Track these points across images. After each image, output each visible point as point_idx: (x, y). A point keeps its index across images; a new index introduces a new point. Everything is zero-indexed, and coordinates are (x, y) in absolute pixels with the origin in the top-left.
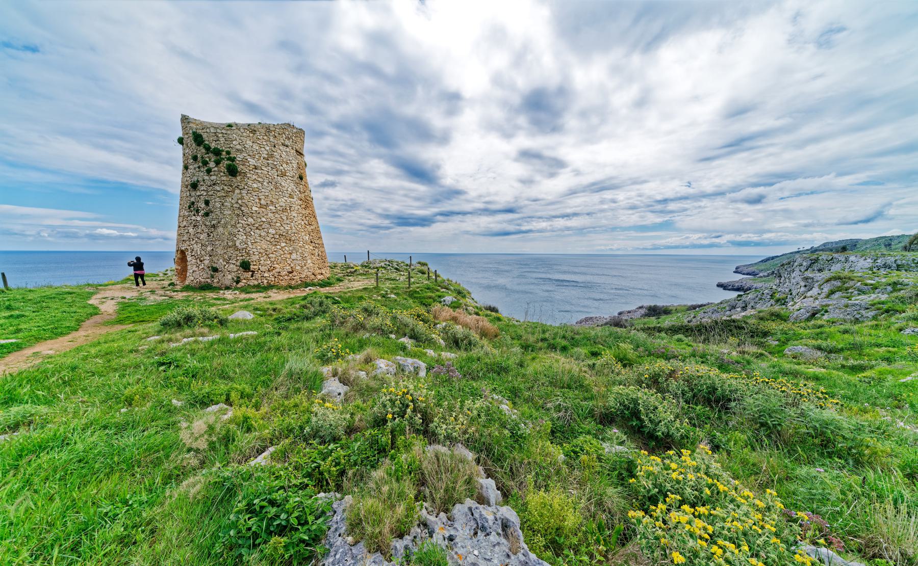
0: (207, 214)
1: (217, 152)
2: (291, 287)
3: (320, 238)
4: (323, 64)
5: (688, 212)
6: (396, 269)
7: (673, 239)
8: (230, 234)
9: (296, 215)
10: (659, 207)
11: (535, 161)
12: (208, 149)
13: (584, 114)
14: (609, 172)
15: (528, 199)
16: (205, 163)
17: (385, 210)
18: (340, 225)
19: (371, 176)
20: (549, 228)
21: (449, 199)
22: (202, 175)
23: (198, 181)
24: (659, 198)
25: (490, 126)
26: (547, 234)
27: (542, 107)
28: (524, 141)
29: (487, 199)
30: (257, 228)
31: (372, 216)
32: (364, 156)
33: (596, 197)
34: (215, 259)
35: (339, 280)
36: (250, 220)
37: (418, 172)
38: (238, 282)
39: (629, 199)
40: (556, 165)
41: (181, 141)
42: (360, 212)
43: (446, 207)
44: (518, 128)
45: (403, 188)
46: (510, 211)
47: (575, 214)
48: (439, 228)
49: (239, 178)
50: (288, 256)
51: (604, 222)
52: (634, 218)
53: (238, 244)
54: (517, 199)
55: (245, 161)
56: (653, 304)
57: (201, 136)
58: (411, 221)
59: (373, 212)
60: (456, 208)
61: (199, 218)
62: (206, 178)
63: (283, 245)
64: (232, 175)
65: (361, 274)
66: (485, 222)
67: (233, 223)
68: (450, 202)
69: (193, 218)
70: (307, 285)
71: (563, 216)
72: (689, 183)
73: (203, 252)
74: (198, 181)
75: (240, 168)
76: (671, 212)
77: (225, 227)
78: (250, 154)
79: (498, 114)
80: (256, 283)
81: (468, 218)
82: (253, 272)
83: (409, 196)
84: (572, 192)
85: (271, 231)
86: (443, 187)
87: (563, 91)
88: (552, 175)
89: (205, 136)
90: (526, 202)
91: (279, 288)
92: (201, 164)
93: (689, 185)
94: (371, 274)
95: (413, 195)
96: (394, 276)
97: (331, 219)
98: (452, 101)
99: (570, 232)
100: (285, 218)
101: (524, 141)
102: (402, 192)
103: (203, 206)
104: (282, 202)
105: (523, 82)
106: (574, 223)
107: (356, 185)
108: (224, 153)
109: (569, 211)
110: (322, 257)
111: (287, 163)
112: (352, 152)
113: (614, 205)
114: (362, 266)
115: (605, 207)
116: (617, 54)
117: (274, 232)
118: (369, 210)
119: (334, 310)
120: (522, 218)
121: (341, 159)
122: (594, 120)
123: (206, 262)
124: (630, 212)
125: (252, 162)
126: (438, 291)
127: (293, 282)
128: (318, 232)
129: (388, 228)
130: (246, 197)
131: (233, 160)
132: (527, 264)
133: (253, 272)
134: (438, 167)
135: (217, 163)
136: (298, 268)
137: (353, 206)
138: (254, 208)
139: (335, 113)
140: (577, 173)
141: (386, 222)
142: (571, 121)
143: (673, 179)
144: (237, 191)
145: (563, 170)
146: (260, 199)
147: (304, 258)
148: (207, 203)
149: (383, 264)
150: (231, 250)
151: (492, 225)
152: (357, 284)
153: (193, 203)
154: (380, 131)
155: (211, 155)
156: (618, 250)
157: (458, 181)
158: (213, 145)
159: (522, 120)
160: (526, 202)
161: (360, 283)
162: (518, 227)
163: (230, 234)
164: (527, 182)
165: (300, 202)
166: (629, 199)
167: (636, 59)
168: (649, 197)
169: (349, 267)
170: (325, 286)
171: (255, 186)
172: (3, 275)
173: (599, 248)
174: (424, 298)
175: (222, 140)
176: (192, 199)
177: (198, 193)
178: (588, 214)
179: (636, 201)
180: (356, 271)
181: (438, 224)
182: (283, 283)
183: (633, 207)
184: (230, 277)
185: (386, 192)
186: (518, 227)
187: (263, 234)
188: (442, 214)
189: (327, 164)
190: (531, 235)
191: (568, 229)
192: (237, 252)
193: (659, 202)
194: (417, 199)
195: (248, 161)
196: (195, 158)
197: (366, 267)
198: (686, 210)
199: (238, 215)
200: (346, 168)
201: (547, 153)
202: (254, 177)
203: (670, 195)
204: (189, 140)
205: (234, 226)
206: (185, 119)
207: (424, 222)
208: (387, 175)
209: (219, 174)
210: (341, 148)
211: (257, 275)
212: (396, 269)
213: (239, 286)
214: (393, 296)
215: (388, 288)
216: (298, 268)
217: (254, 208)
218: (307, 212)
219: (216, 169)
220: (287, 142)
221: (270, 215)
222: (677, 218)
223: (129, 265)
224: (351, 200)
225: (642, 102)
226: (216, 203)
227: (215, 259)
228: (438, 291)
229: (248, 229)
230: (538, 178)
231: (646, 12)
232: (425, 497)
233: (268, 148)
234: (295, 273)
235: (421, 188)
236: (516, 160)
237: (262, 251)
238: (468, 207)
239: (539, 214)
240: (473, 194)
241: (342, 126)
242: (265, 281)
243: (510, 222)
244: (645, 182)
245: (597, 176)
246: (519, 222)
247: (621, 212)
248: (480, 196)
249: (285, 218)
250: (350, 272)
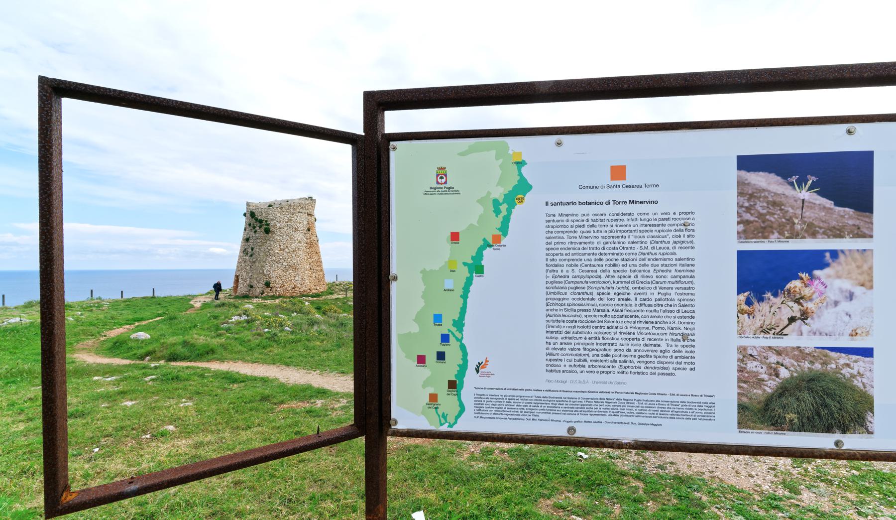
0: (251, 256)
1: (261, 221)
12: (256, 219)
16: (254, 227)
22: (252, 234)
75: (272, 229)
77: (259, 262)
78: (277, 220)
125: (278, 225)
131: (268, 225)
135: (260, 227)
147: (303, 279)
148: (252, 249)
150: (261, 276)
155: (259, 223)
172: (3, 296)
195: (275, 224)
196: (250, 225)
204: (248, 215)
205: (264, 262)
206: (248, 204)
209: (261, 233)
211: (274, 290)
223: (465, 264)
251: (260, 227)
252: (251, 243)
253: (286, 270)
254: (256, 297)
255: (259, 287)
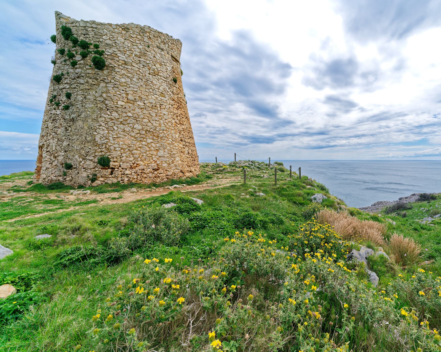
0: (67, 108)
1: (85, 46)
2: (155, 185)
3: (192, 138)
4: (208, 49)
5: (437, 133)
6: (258, 168)
7: (428, 150)
8: (90, 128)
9: (166, 113)
10: (417, 130)
11: (337, 103)
12: (75, 42)
13: (365, 75)
14: (382, 109)
15: (333, 126)
16: (71, 56)
17: (244, 133)
18: (216, 143)
19: (236, 113)
20: (347, 144)
21: (283, 126)
23: (62, 75)
24: (416, 124)
25: (308, 82)
26: (346, 148)
27: (339, 71)
28: (329, 91)
29: (307, 126)
30: (121, 123)
31: (236, 137)
32: (231, 101)
33: (376, 125)
34: (70, 155)
35: (209, 178)
36: (115, 114)
37: (265, 111)
38: (93, 180)
39: (397, 125)
40: (349, 106)
41: (54, 39)
42: (229, 135)
43: (282, 131)
44: (325, 84)
45: (255, 120)
46: (321, 133)
47: (363, 135)
48: (278, 144)
49: (105, 72)
50: (155, 153)
51: (382, 140)
52: (401, 137)
53: (97, 139)
54: (326, 125)
55: (113, 56)
56: (422, 193)
57: (70, 30)
58: (260, 140)
59: (237, 135)
60: (288, 132)
61: (58, 112)
62: (71, 70)
63: (149, 141)
64: (97, 68)
65: (228, 172)
66: (306, 140)
67: (94, 116)
68: (284, 128)
69: (54, 112)
70: (173, 183)
71: (356, 136)
72: (434, 115)
73: (58, 148)
74: (62, 75)
76: (425, 133)
77: (85, 120)
78: (119, 53)
79: (313, 76)
80: (115, 181)
81: (296, 138)
82: (113, 169)
83: (258, 126)
84: (361, 122)
85: (136, 126)
86: (280, 119)
87: (351, 62)
88: (347, 111)
89: (74, 30)
90: (332, 128)
91: (139, 186)
92: (67, 58)
93: (435, 116)
94: (238, 172)
95: (261, 124)
96: (258, 173)
97: (211, 139)
98: (285, 69)
99: (361, 146)
100: (154, 115)
101: (329, 91)
102: (255, 123)
103: (64, 99)
104: (152, 99)
105: (327, 57)
106: (363, 140)
107: (226, 118)
108: (92, 47)
109: (359, 133)
110: (194, 157)
111: (161, 65)
112: (224, 99)
113: (388, 129)
114: (230, 165)
115: (382, 130)
116: (381, 41)
117: (140, 127)
118: (234, 134)
119: (190, 217)
120: (330, 138)
121: (217, 103)
122: (371, 78)
123: (60, 158)
124: (399, 133)
125: (122, 57)
126: (304, 187)
127: (158, 180)
128: (190, 132)
129: (246, 144)
130: (112, 91)
132: (334, 165)
133: (113, 169)
134: (277, 107)
135: (84, 56)
136: (165, 165)
137: (224, 131)
138: (120, 103)
139: (215, 77)
140: (362, 110)
141: (245, 141)
142: (357, 80)
143: (423, 113)
144: (102, 84)
145: (354, 109)
146: (127, 94)
147: (172, 155)
148: (68, 96)
149: (247, 164)
151: (311, 142)
152: (225, 182)
153: (55, 97)
154: (241, 86)
155: (81, 50)
156: (393, 157)
157: (289, 116)
158: (81, 38)
159: (327, 79)
160: (332, 128)
161: (228, 180)
162: (328, 144)
163: (90, 128)
164: (332, 115)
165: (173, 102)
166: (397, 125)
167: (394, 44)
168: (410, 124)
169: (219, 166)
170: (193, 184)
171: (123, 80)
173: (380, 156)
174: (293, 195)
175: (91, 34)
176: (55, 93)
177: (61, 87)
178: (371, 135)
179: (401, 127)
180: (224, 169)
181: (277, 142)
182: (146, 181)
183: (400, 131)
184: (85, 174)
185: (245, 123)
186: (328, 144)
187: (127, 129)
188: (279, 136)
189: (209, 106)
190: (336, 148)
191: (360, 144)
192: (96, 148)
193: (417, 127)
194: (264, 127)
197: (233, 166)
198: (435, 132)
199: (101, 109)
200: (220, 108)
201: (343, 98)
202: (123, 72)
203: (423, 122)
204: (60, 37)
205: (96, 120)
206: (58, 15)
207: (269, 140)
208: (245, 112)
209: (85, 67)
210: (218, 97)
211: (117, 173)
212: (258, 168)
213: (94, 184)
214: (262, 194)
215: (255, 185)
216: (165, 165)
217: (120, 103)
218: (179, 112)
219: (82, 62)
220: (162, 46)
221: (137, 110)
222: (430, 137)
224: (223, 127)
225: (399, 67)
226: (78, 97)
227: (70, 155)
228: (304, 187)
229: (110, 124)
230: (339, 113)
231: (400, 13)
232: (267, 330)
233: (141, 47)
234: (161, 171)
235: (266, 120)
236: (325, 102)
237: (124, 147)
238: (296, 131)
239: (340, 135)
240: (299, 123)
241: (219, 84)
242: (126, 179)
243: (322, 140)
244: (405, 115)
245: (376, 111)
246: (328, 140)
247: (393, 133)
248: (303, 125)
249: (154, 115)
250: (219, 169)
251: (84, 56)
252: (64, 85)
253: (141, 137)
254: (81, 187)
255: (86, 168)
